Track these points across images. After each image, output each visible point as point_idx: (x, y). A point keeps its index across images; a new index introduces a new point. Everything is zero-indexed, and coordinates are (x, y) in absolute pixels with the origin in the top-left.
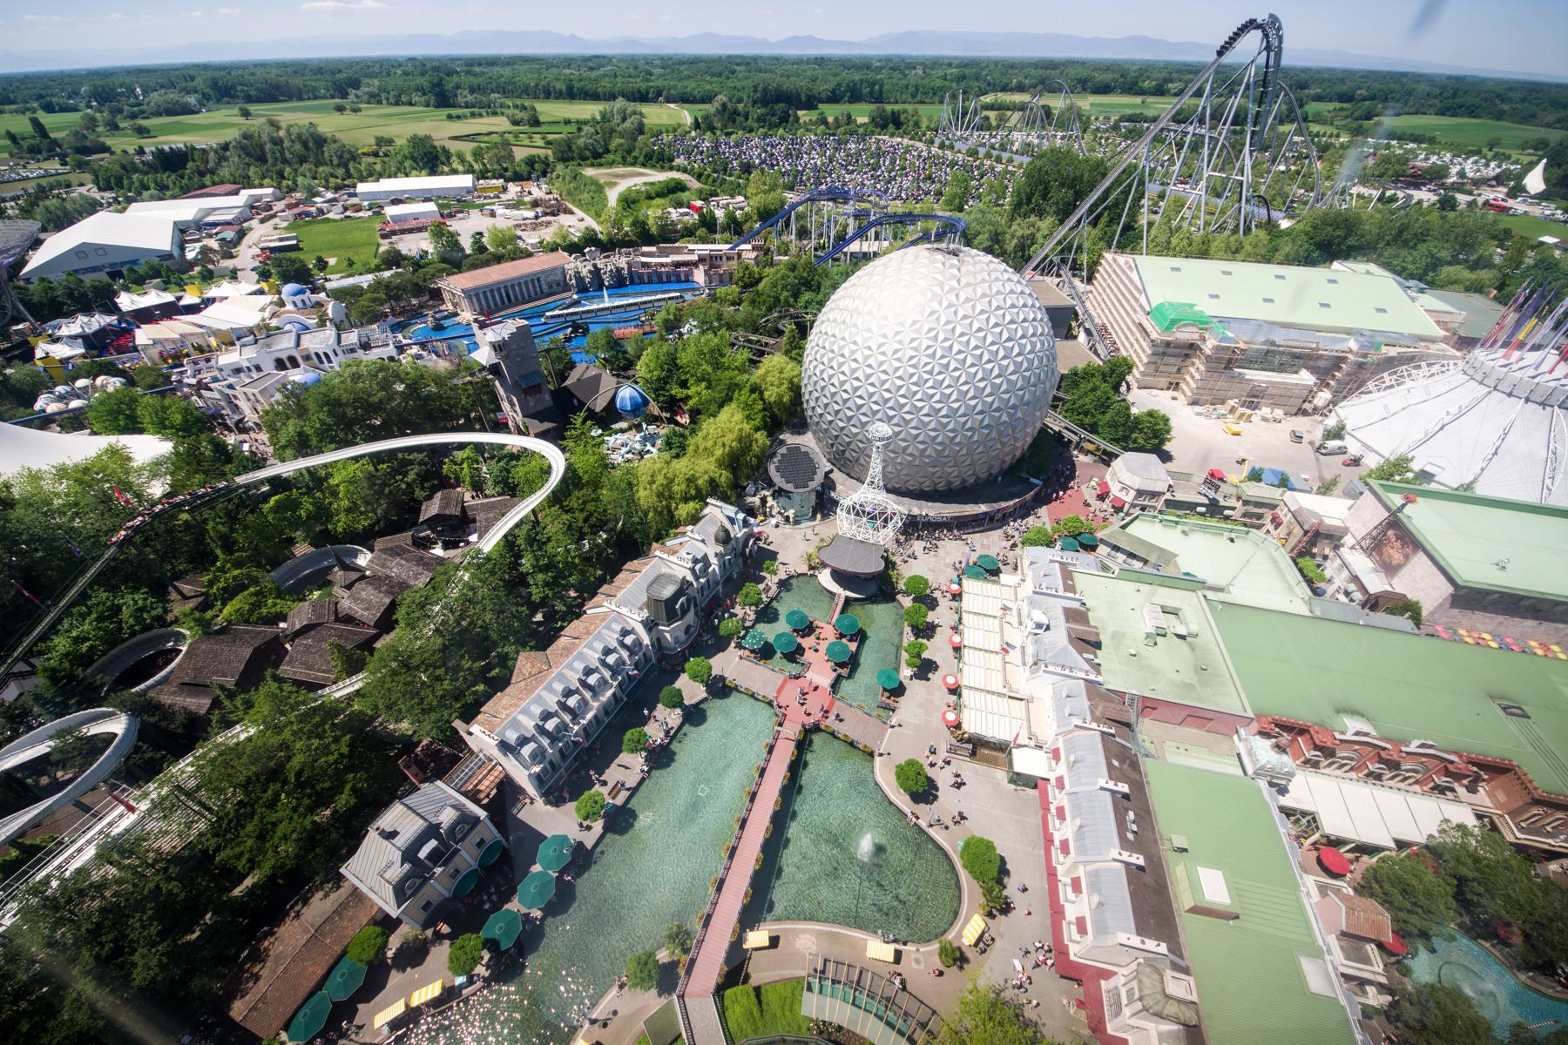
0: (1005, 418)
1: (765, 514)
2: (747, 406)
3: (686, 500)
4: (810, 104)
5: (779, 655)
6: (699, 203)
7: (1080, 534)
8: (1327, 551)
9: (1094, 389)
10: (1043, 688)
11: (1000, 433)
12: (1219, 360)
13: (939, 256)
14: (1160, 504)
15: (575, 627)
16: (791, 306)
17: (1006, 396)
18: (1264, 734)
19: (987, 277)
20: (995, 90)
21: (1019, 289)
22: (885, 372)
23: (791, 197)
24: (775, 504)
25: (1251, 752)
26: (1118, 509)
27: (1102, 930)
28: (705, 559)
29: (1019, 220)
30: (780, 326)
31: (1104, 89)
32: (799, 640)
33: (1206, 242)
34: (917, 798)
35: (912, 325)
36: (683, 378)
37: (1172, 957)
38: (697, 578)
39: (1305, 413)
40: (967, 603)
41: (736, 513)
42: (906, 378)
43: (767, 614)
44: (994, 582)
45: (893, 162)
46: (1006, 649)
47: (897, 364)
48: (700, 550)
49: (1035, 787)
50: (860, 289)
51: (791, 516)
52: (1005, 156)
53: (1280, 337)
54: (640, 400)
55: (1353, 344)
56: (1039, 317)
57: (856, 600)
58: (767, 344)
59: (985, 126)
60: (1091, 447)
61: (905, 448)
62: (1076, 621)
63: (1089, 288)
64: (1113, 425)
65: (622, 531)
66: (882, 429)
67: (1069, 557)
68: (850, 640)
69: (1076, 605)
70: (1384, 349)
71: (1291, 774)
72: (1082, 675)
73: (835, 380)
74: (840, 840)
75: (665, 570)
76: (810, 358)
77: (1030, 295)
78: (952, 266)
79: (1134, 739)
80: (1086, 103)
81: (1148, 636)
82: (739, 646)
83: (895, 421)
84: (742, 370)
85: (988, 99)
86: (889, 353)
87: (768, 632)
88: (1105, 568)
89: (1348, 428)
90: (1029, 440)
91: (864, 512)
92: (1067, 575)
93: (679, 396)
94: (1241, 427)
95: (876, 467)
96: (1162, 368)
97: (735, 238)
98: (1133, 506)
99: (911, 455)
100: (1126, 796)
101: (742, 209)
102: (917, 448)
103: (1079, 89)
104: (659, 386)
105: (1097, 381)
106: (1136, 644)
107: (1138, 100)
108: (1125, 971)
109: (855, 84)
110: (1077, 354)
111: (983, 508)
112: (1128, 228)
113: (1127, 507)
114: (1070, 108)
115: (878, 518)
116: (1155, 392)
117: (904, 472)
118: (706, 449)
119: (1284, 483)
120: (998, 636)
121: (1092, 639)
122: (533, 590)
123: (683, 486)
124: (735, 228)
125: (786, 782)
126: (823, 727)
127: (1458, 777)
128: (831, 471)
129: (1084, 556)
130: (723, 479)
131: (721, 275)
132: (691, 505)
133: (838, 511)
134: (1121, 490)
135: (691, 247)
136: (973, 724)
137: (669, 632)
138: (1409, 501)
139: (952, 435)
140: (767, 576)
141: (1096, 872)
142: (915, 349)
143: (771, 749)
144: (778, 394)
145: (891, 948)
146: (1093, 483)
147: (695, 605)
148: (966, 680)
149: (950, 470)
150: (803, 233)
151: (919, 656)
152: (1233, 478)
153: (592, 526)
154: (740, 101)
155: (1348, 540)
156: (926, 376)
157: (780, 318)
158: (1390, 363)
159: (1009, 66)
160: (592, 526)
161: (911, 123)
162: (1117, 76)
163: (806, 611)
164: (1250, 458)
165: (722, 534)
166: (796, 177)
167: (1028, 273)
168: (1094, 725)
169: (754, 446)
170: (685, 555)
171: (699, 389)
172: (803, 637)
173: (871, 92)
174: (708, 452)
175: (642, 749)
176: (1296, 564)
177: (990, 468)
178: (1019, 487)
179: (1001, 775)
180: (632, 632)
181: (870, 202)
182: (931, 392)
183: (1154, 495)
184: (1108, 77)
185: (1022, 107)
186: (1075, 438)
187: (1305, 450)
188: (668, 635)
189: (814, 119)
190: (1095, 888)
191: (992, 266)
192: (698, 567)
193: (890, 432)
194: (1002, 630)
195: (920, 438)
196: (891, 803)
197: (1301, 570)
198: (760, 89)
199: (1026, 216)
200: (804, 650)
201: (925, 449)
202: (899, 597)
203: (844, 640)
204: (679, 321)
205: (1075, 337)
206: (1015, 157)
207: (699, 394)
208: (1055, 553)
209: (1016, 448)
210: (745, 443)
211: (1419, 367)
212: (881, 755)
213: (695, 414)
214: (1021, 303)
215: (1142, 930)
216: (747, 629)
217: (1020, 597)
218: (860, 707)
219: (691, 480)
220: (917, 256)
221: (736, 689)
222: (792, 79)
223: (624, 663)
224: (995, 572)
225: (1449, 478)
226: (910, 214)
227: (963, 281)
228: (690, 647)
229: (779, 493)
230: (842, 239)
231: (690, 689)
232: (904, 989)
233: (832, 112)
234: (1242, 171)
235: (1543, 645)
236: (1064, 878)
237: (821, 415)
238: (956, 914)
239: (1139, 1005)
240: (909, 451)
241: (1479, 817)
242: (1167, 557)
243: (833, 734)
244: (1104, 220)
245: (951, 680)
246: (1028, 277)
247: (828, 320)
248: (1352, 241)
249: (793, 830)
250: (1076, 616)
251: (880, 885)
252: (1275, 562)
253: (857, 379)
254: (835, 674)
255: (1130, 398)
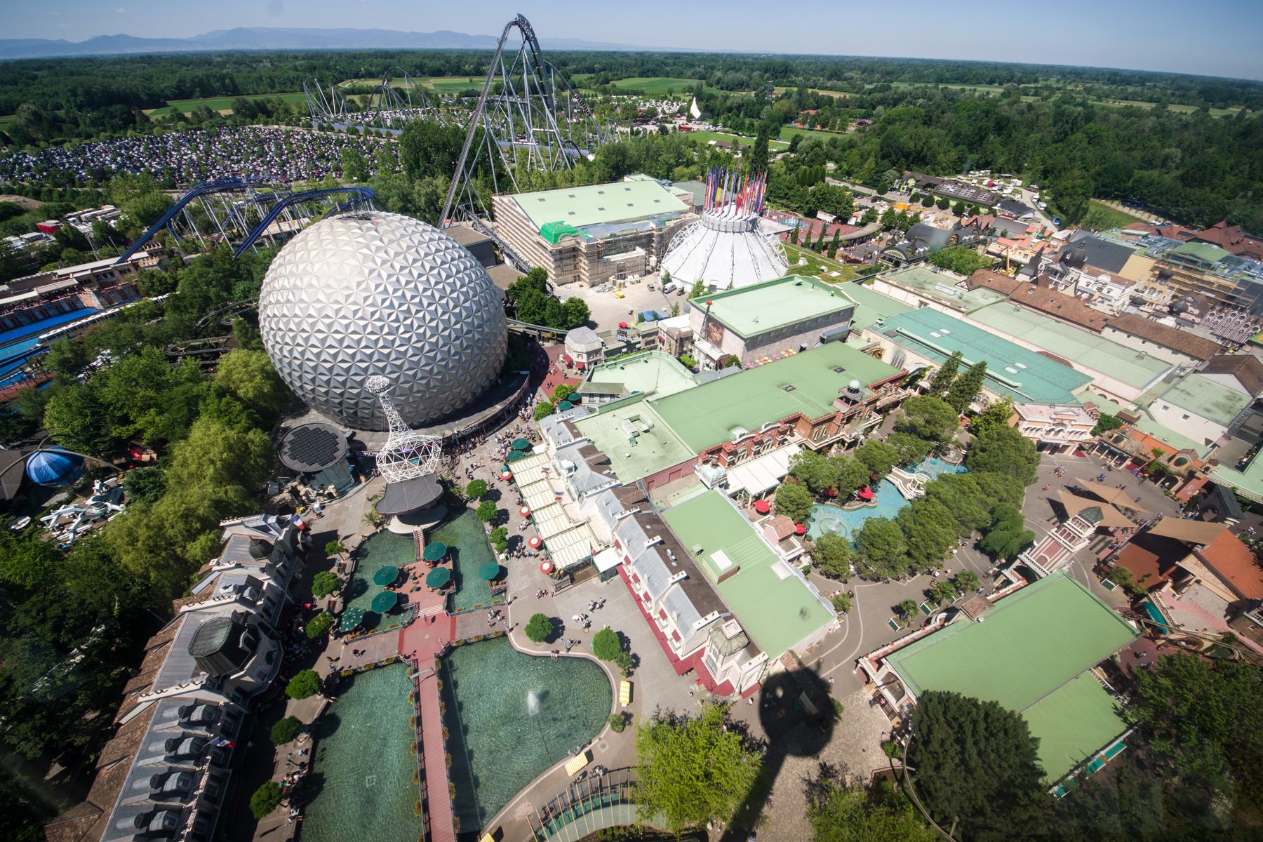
0: (477, 336)
1: (303, 503)
2: (220, 413)
3: (192, 536)
4: (157, 101)
5: (384, 616)
6: (51, 223)
7: (568, 396)
8: (690, 347)
9: (530, 296)
10: (591, 508)
11: (480, 349)
12: (592, 254)
13: (353, 223)
14: (603, 357)
15: (111, 750)
16: (226, 300)
17: (469, 320)
18: (706, 462)
19: (404, 232)
20: (348, 77)
21: (436, 236)
22: (354, 332)
23: (176, 196)
24: (308, 489)
25: (704, 475)
26: (583, 369)
27: (686, 629)
28: (252, 582)
29: (417, 182)
30: (224, 322)
31: (438, 73)
32: (398, 591)
33: (552, 177)
34: (550, 639)
35: (376, 289)
36: (119, 414)
37: (723, 615)
38: (251, 604)
39: (648, 272)
40: (520, 481)
41: (265, 520)
42: (378, 332)
43: (354, 589)
44: (531, 456)
45: (279, 147)
46: (559, 497)
47: (362, 323)
48: (240, 576)
49: (617, 573)
50: (289, 267)
51: (333, 491)
52: (383, 131)
53: (617, 230)
54: (66, 461)
55: (652, 225)
56: (463, 254)
57: (433, 528)
58: (217, 344)
59: (352, 108)
60: (549, 335)
61: (411, 388)
62: (590, 454)
63: (495, 224)
64: (553, 316)
65: (122, 614)
66: (377, 382)
67: (567, 414)
68: (445, 562)
69: (585, 444)
70: (667, 223)
71: (725, 475)
72: (608, 486)
73: (309, 355)
74: (513, 714)
75: (204, 620)
76: (270, 343)
77: (447, 239)
78: (369, 229)
79: (652, 506)
80: (430, 84)
81: (631, 440)
82: (339, 635)
83: (388, 369)
84: (195, 379)
85: (347, 85)
86: (350, 315)
87: (363, 604)
88: (592, 411)
89: (671, 274)
90: (504, 345)
91: (402, 455)
92: (572, 427)
93: (125, 436)
94: (623, 292)
95: (391, 414)
96: (565, 269)
97: (121, 249)
98: (589, 364)
99: (418, 391)
100: (662, 542)
101: (114, 218)
102: (421, 384)
103: (419, 74)
104: (91, 435)
105: (529, 289)
106: (628, 449)
107: (467, 80)
108: (707, 643)
109: (201, 80)
110: (505, 276)
111: (498, 407)
112: (501, 176)
113: (586, 366)
114: (418, 89)
115: (418, 453)
116: (569, 285)
117: (421, 407)
118: (191, 475)
119: (656, 317)
120: (550, 491)
121: (603, 460)
122: (24, 746)
123: (181, 525)
124: (114, 239)
125: (444, 711)
126: (454, 645)
127: (784, 433)
128: (354, 434)
129: (577, 409)
130: (231, 494)
131: (121, 292)
132: (202, 538)
133: (378, 464)
134: (578, 356)
135: (60, 272)
136: (562, 561)
137: (243, 675)
138: (710, 304)
139: (443, 363)
140: (337, 556)
141: (669, 600)
142: (372, 305)
143: (417, 697)
144: (255, 388)
145: (582, 755)
146: (561, 359)
147: (266, 630)
148: (544, 535)
149: (458, 390)
150: (208, 228)
151: (504, 539)
152: (632, 324)
153: (71, 631)
154: (59, 107)
155: (696, 337)
156: (396, 325)
157: (220, 315)
158: (673, 231)
159: (353, 57)
160: (71, 631)
161: (280, 111)
162: (443, 62)
163: (393, 564)
164: (635, 309)
165: (258, 548)
166: (172, 175)
167: (446, 222)
168: (628, 513)
169: (253, 448)
170: (222, 591)
171: (148, 418)
172: (400, 586)
173: (223, 85)
174: (197, 476)
175: (279, 802)
176: (680, 361)
177: (488, 377)
178: (516, 381)
179: (595, 581)
180: (197, 703)
181: (270, 186)
182: (407, 336)
183: (597, 352)
184: (437, 63)
185: (378, 90)
186: (536, 333)
187: (658, 294)
188: (248, 679)
189: (168, 116)
190: (671, 609)
191: (405, 223)
192: (246, 594)
193: (387, 381)
194: (551, 486)
195: (419, 375)
196: (535, 657)
197: (684, 364)
198: (80, 91)
199: (421, 177)
200: (406, 596)
201: (428, 383)
202: (469, 505)
203: (440, 566)
204: (83, 356)
205: (503, 262)
206: (392, 131)
207: (152, 423)
208: (558, 417)
209: (498, 355)
210: (239, 452)
211: (685, 229)
212: (512, 629)
213: (160, 445)
214: (443, 247)
215: (703, 614)
216: (339, 616)
217: (551, 456)
218: (478, 607)
219: (187, 516)
220: (332, 227)
221: (356, 673)
222: (119, 79)
223: (206, 740)
224: (529, 448)
225: (722, 285)
226: (315, 191)
227: (386, 240)
228: (283, 671)
229: (307, 478)
230: (257, 225)
231: (303, 708)
232: (606, 771)
233: (188, 108)
234: (551, 127)
235: (787, 352)
236: (655, 616)
237: (313, 390)
238: (611, 693)
239: (721, 657)
240: (415, 389)
241: (800, 446)
242: (620, 386)
243: (466, 644)
244: (480, 172)
245: (535, 541)
246: (447, 225)
247: (270, 303)
248: (628, 162)
249: (471, 741)
250: (588, 450)
251: (555, 720)
252: (670, 364)
253: (331, 347)
254: (444, 597)
255: (556, 293)
